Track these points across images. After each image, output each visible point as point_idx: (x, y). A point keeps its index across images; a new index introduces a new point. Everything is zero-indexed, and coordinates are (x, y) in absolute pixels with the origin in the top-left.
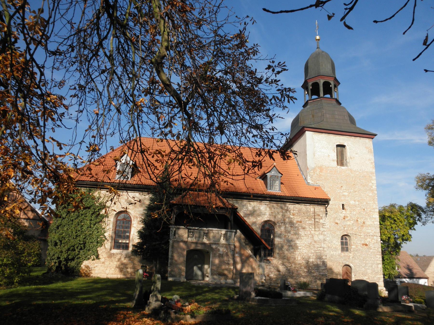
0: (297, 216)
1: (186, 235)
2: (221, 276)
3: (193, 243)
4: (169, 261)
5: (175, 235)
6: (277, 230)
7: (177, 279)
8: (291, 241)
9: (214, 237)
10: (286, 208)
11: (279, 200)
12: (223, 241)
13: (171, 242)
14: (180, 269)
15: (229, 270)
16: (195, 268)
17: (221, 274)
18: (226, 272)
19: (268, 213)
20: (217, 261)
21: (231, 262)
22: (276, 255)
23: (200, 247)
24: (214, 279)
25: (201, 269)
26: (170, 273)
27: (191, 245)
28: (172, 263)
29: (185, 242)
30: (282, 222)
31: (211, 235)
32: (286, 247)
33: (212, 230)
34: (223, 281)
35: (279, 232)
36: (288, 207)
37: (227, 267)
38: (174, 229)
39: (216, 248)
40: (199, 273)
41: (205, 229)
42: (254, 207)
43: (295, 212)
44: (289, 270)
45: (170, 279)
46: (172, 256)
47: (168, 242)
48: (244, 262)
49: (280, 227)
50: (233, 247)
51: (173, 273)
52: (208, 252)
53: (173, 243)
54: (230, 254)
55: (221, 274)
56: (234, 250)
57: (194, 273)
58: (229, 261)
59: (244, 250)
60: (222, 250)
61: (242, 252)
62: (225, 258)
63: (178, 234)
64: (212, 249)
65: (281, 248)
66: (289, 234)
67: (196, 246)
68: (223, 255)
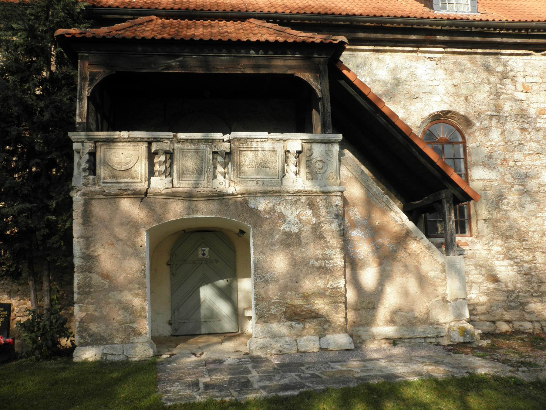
0: (538, 92)
1: (141, 168)
2: (298, 321)
3: (174, 195)
4: (77, 279)
5: (92, 169)
6: (476, 141)
7: (116, 352)
8: (527, 176)
9: (261, 166)
10: (500, 69)
11: (478, 39)
12: (298, 181)
13: (77, 198)
14: (127, 308)
15: (335, 297)
16: (206, 293)
17: (298, 316)
18: (321, 305)
19: (441, 89)
20: (279, 263)
21: (338, 260)
22: (479, 225)
23: (204, 212)
24: (275, 336)
25: (228, 294)
26: (83, 330)
27: (165, 206)
28: (90, 286)
29: (142, 196)
30: (492, 116)
31: (248, 159)
32: (512, 197)
33: (251, 140)
34: (310, 343)
35: (485, 150)
36: (505, 65)
37: (320, 283)
38: (89, 146)
39: (272, 210)
40: (223, 308)
41: (218, 136)
42: (394, 71)
43: (529, 80)
44: (528, 274)
45: (89, 354)
46: (89, 258)
47: (69, 202)
48: (386, 258)
49: (486, 130)
50: (337, 201)
51: (94, 327)
52: (242, 232)
53: (87, 204)
54: (330, 228)
55: (298, 316)
56: (340, 217)
57: (203, 311)
58: (326, 258)
59: (384, 212)
60: (297, 216)
61: (378, 219)
62: (313, 250)
63: (106, 163)
64: (254, 213)
65: (498, 200)
66: (517, 155)
67: (190, 210)
68: (298, 235)
